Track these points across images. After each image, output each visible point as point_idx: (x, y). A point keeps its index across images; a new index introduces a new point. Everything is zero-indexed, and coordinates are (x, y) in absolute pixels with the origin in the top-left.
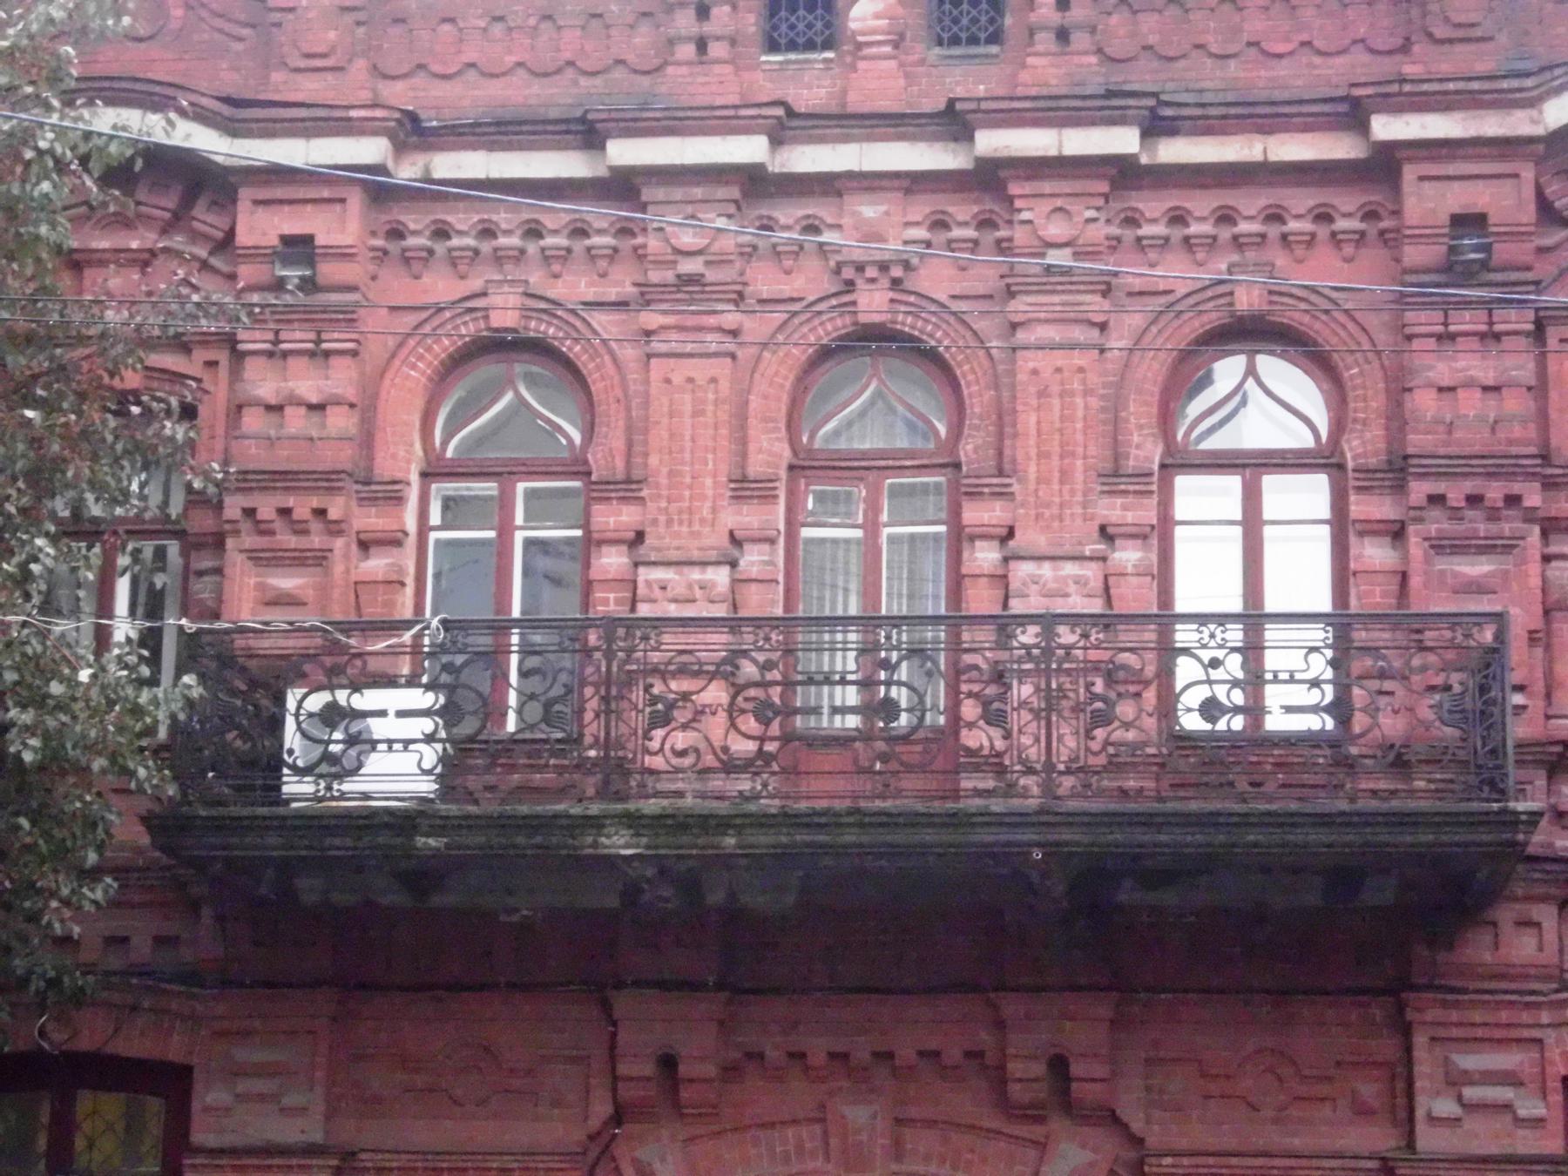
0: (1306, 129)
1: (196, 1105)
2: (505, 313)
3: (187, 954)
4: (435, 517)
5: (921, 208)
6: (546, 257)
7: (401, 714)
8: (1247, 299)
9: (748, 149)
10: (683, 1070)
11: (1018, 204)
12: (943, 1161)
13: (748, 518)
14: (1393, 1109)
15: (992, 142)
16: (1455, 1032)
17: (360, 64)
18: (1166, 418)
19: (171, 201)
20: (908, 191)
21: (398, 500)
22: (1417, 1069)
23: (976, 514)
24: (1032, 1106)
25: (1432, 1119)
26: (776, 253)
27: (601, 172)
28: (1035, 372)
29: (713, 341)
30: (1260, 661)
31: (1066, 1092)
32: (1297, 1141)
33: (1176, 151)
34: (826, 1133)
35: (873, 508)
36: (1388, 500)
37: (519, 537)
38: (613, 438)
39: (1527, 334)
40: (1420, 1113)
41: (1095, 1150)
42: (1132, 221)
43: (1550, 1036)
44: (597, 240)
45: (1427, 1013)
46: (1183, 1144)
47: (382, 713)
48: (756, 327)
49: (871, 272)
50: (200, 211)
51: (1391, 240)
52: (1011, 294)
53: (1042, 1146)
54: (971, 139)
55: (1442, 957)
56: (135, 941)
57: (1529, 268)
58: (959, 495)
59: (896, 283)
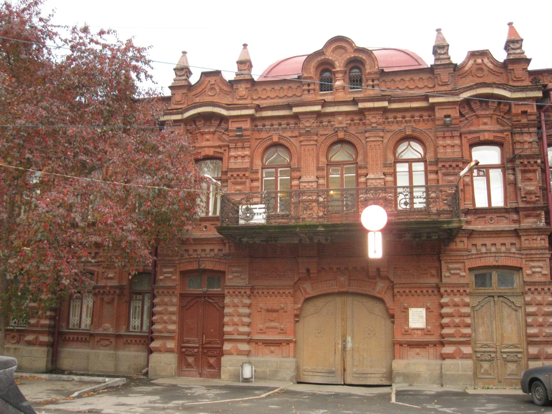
0: (417, 101)
1: (226, 278)
2: (275, 139)
3: (224, 252)
4: (264, 176)
5: (349, 118)
6: (283, 129)
7: (259, 208)
9: (317, 108)
14: (438, 275)
15: (361, 105)
16: (449, 261)
17: (250, 97)
19: (218, 122)
23: (361, 172)
25: (445, 276)
29: (312, 143)
30: (413, 194)
33: (394, 106)
37: (279, 178)
38: (295, 160)
40: (443, 275)
45: (444, 258)
46: (401, 282)
47: (256, 208)
49: (340, 129)
50: (222, 124)
51: (434, 120)
54: (357, 105)
55: (446, 248)
57: (458, 124)
58: (358, 168)
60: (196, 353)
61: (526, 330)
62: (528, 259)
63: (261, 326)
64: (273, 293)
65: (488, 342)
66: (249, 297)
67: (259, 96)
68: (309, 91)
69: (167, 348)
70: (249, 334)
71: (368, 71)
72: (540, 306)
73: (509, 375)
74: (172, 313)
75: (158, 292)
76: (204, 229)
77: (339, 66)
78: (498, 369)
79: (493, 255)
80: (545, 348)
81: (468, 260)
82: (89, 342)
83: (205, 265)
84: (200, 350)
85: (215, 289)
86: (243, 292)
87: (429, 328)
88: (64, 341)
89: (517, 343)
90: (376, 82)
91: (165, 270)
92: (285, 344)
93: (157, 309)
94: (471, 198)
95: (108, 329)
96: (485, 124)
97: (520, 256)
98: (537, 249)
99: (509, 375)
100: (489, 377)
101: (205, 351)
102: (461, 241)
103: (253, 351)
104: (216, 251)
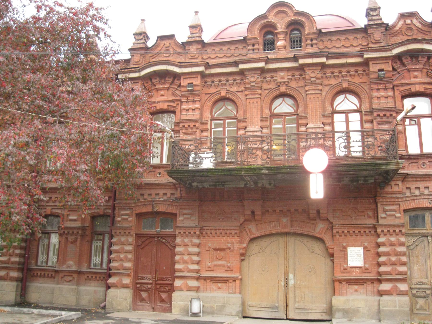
1: (178, 219)
2: (223, 93)
3: (176, 196)
4: (213, 127)
5: (290, 73)
8: (345, 85)
9: (261, 65)
10: (255, 213)
11: (306, 71)
12: (299, 227)
13: (264, 124)
14: (374, 216)
16: (385, 203)
18: (332, 105)
19: (171, 80)
20: (288, 71)
21: (206, 123)
22: (379, 209)
24: (314, 218)
25: (381, 217)
26: (267, 81)
27: (238, 70)
28: (310, 98)
29: (257, 96)
31: (320, 215)
32: (358, 222)
34: (279, 224)
35: (284, 121)
36: (370, 116)
37: (226, 129)
38: (241, 112)
39: (391, 88)
40: (379, 217)
41: (325, 225)
42: (325, 74)
43: (401, 203)
44: (237, 81)
45: (380, 201)
46: (340, 223)
48: (265, 93)
49: (282, 83)
50: (176, 81)
51: (368, 75)
52: (305, 86)
53: (315, 224)
54: (298, 61)
55: (382, 191)
56: (168, 194)
57: (391, 78)
59: (286, 85)
60: (149, 288)
63: (209, 264)
64: (221, 233)
66: (198, 237)
67: (209, 56)
68: (253, 50)
69: (123, 284)
70: (198, 271)
71: (307, 31)
74: (128, 252)
75: (116, 232)
76: (158, 176)
77: (281, 27)
82: (54, 278)
83: (158, 208)
84: (154, 286)
85: (167, 230)
86: (192, 232)
87: (367, 266)
88: (32, 277)
90: (314, 42)
91: (122, 212)
92: (231, 281)
93: (114, 248)
94: (405, 145)
95: (71, 266)
96: (416, 77)
101: (158, 287)
102: (396, 185)
103: (202, 288)
104: (169, 195)
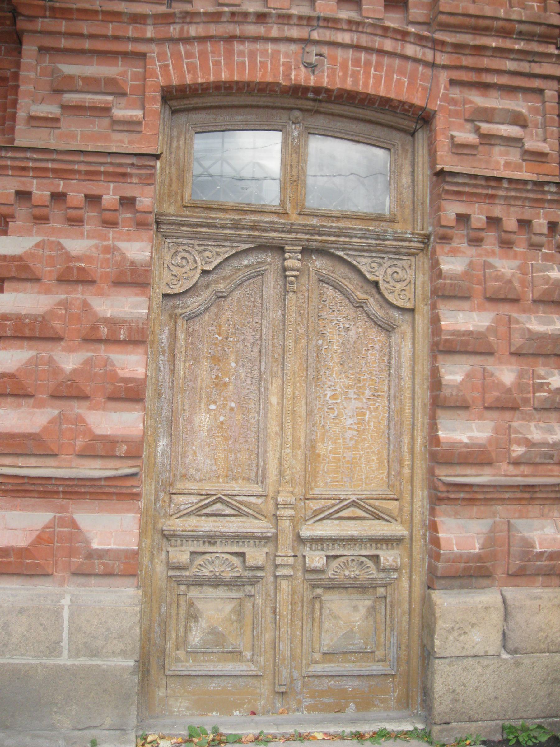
16: (64, 43)
61: (433, 427)
62: (464, 76)
65: (236, 487)
72: (506, 309)
73: (328, 656)
78: (276, 625)
79: (295, 33)
80: (520, 524)
81: (167, 48)
89: (383, 491)
97: (429, 55)
98: (505, 33)
99: (328, 656)
100: (230, 667)
